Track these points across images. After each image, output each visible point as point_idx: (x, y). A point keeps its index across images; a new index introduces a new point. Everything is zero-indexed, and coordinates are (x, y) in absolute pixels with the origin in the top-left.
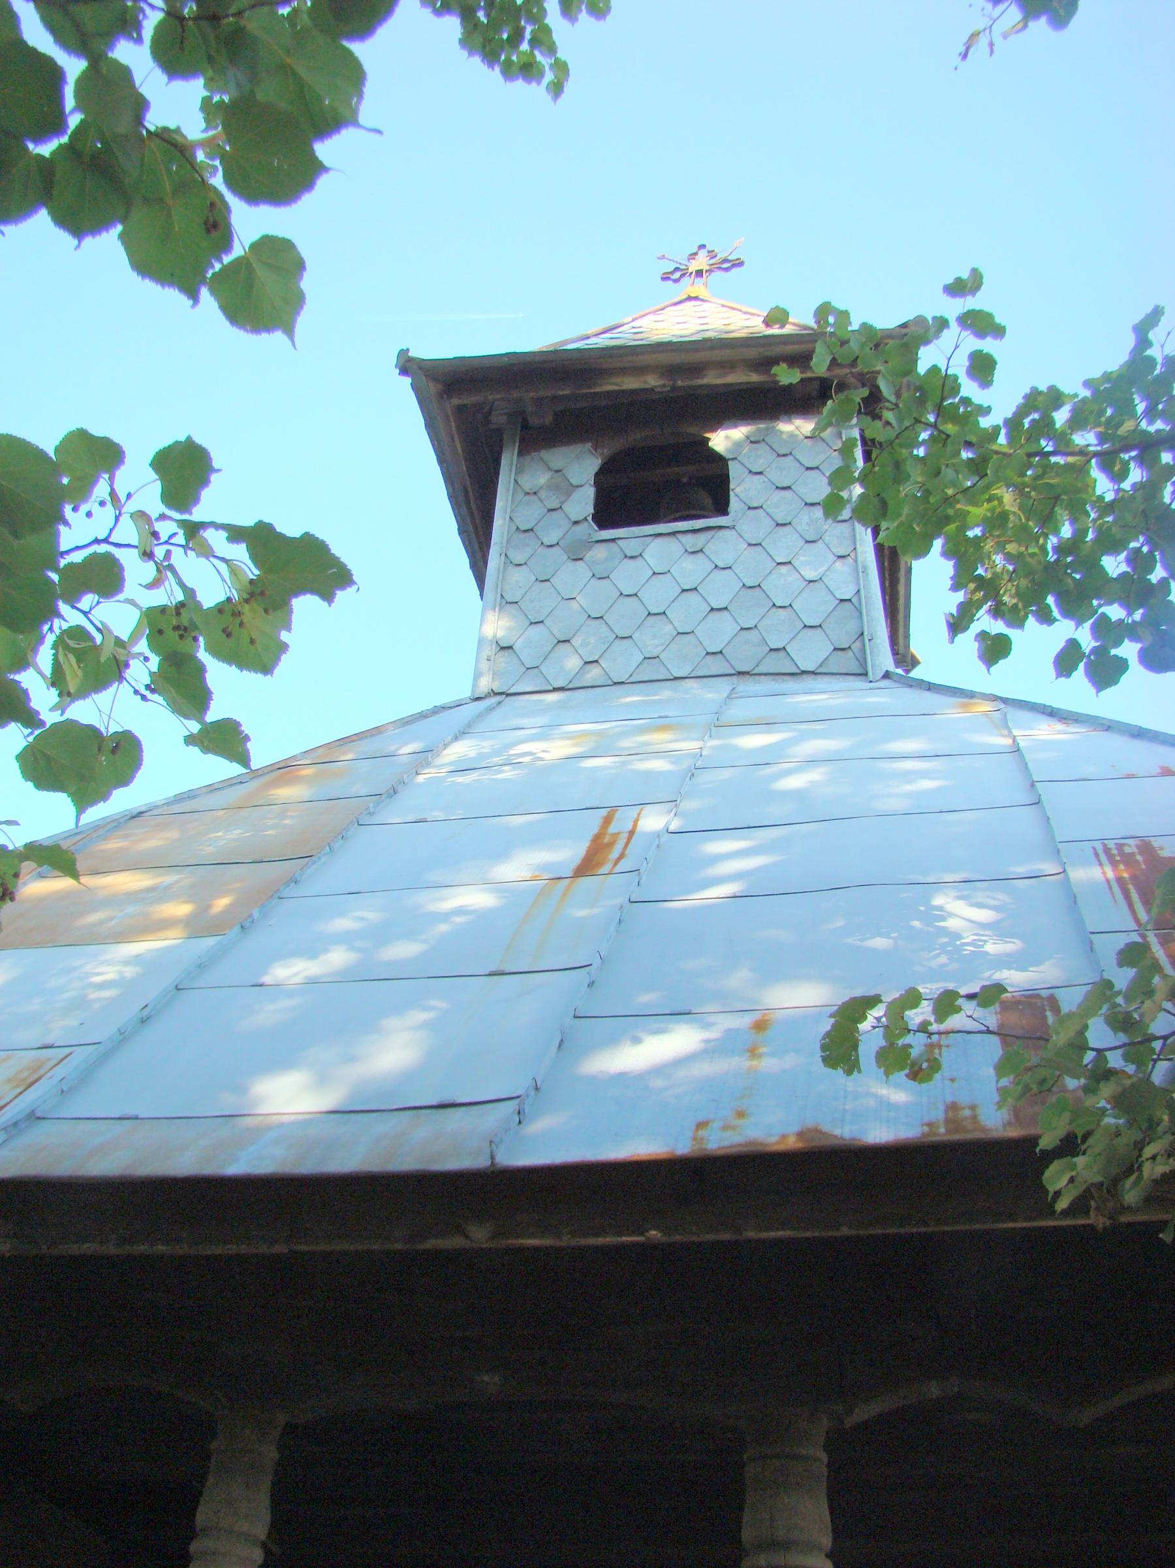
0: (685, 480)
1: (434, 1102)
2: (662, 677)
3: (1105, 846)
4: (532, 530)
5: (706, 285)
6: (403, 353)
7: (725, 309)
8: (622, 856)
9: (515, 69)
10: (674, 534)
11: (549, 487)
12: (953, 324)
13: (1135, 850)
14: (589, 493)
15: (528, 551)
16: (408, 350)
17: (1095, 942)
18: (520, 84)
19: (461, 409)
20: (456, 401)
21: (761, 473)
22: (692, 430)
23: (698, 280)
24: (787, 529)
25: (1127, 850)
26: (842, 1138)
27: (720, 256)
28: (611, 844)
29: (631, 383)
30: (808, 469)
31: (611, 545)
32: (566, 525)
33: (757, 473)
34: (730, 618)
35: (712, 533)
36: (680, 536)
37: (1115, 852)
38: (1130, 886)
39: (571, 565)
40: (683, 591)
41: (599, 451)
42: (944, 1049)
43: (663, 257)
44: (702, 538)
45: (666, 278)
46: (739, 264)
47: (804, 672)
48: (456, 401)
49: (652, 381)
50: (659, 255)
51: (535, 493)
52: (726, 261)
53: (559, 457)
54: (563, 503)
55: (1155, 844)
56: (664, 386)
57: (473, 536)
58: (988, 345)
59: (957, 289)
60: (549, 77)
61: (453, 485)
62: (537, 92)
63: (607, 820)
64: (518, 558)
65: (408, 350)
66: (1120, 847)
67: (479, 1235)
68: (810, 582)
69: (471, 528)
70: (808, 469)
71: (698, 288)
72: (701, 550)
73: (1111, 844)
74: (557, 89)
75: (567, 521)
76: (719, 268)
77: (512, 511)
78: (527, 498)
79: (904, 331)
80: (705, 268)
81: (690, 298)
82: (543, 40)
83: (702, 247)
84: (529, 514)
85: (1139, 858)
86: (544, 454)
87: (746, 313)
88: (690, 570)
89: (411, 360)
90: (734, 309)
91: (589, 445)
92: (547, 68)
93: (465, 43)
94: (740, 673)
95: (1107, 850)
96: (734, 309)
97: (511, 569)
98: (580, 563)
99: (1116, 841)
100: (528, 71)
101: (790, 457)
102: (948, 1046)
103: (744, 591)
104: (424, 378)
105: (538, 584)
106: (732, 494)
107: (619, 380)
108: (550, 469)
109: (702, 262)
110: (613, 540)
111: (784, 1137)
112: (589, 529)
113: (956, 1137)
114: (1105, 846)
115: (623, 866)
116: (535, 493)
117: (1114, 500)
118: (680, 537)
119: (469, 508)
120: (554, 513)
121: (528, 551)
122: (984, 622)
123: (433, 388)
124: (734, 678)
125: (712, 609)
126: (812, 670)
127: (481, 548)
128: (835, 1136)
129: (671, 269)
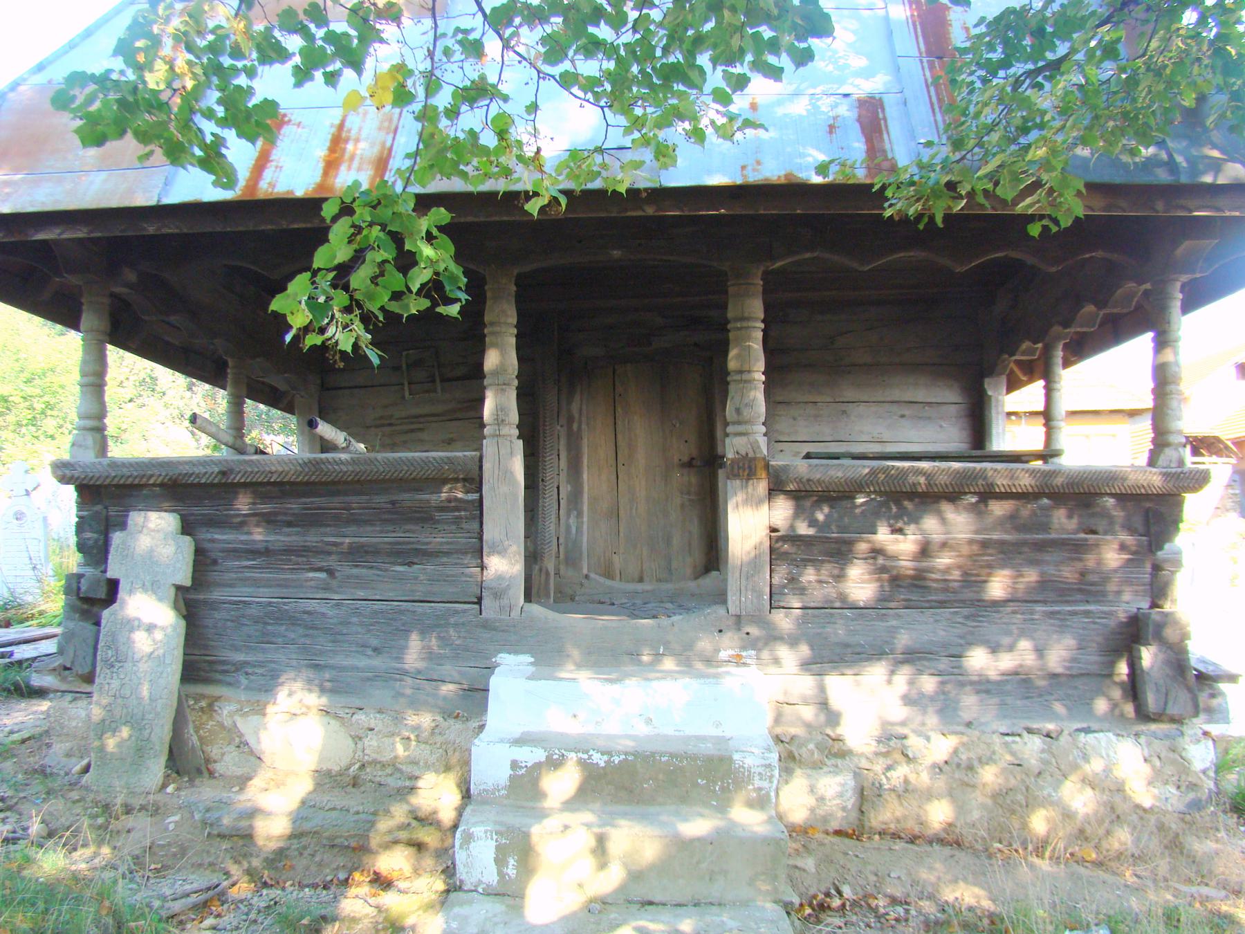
111: (779, 177)
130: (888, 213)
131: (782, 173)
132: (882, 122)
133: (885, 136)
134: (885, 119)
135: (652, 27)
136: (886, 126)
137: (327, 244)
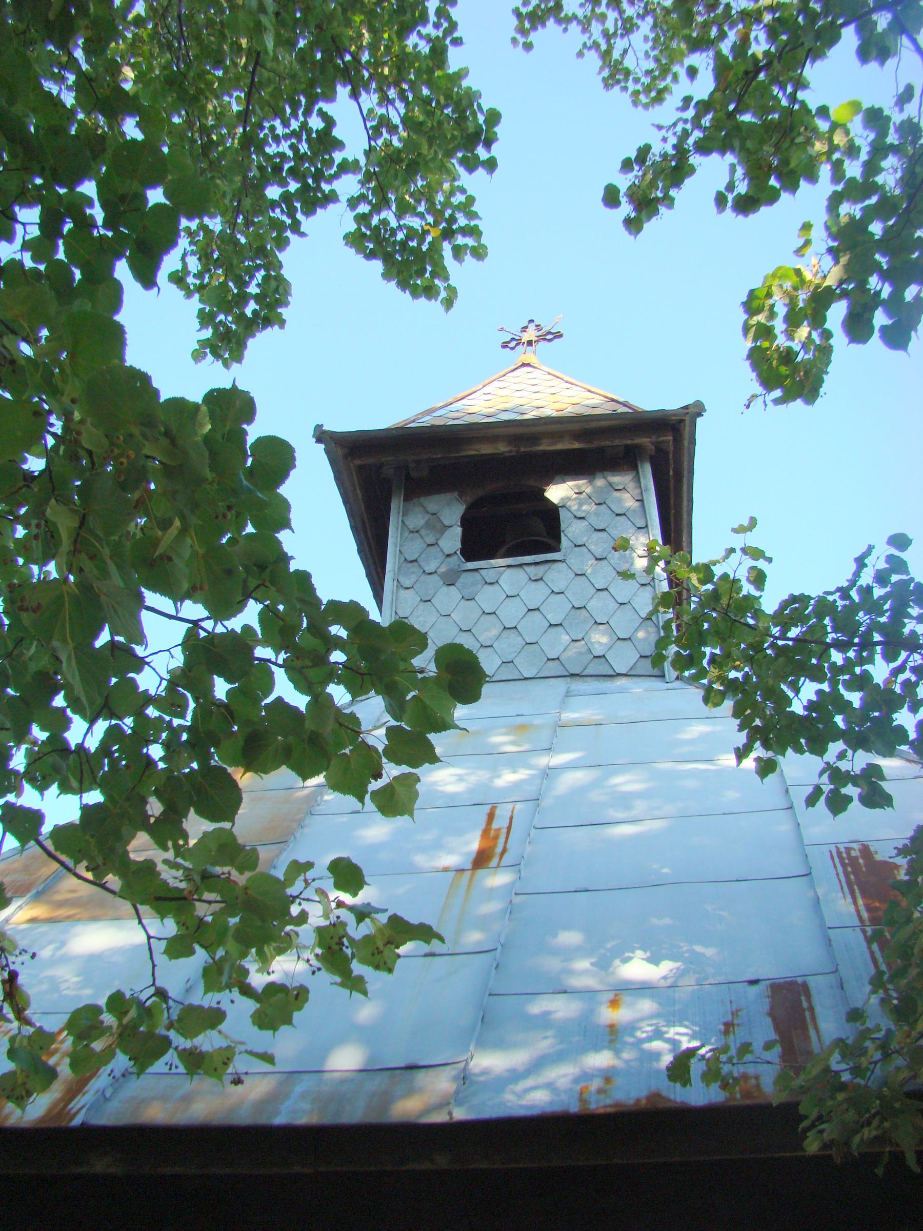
0: (525, 512)
1: (402, 1065)
2: (515, 677)
3: (837, 848)
4: (416, 561)
5: (535, 353)
6: (319, 427)
7: (551, 377)
8: (504, 850)
9: (420, 290)
10: (520, 566)
11: (427, 525)
12: (738, 552)
13: (859, 854)
14: (459, 531)
15: (413, 578)
16: (322, 425)
17: (832, 938)
18: (423, 300)
19: (360, 468)
20: (358, 462)
21: (583, 518)
22: (532, 483)
23: (529, 348)
24: (604, 563)
25: (853, 854)
26: (675, 1102)
27: (545, 329)
28: (496, 838)
29: (486, 449)
30: (618, 515)
31: (476, 574)
32: (441, 557)
33: (580, 518)
34: (564, 631)
35: (549, 565)
36: (525, 568)
37: (844, 855)
38: (856, 887)
39: (445, 589)
40: (529, 610)
41: (464, 498)
42: (736, 1028)
43: (502, 329)
44: (542, 568)
45: (505, 346)
46: (559, 335)
47: (619, 675)
48: (358, 462)
49: (502, 448)
50: (499, 328)
51: (417, 532)
52: (549, 333)
53: (433, 503)
54: (437, 540)
55: (872, 849)
56: (511, 451)
57: (369, 556)
58: (761, 564)
59: (740, 530)
60: (443, 294)
61: (354, 519)
62: (435, 306)
63: (491, 817)
64: (407, 583)
65: (322, 425)
66: (848, 850)
67: (442, 1161)
68: (621, 604)
69: (367, 549)
70: (618, 515)
71: (530, 358)
72: (542, 579)
73: (842, 849)
74: (449, 303)
75: (441, 554)
76: (545, 339)
77: (401, 545)
78: (411, 535)
79: (687, 411)
80: (534, 339)
81: (524, 365)
82: (440, 272)
83: (531, 321)
84: (414, 548)
85: (861, 861)
86: (423, 500)
87: (567, 382)
88: (534, 594)
89: (325, 432)
90: (558, 377)
91: (456, 494)
92: (442, 289)
93: (386, 276)
94: (573, 675)
95: (839, 853)
96: (558, 377)
97: (403, 593)
98: (452, 588)
99: (845, 845)
100: (429, 292)
101: (605, 506)
102: (738, 1025)
103: (573, 611)
104: (333, 445)
105: (422, 604)
106: (562, 534)
107: (477, 447)
108: (427, 512)
109: (531, 335)
110: (476, 570)
111: (638, 1100)
112: (458, 560)
113: (748, 1102)
114: (837, 848)
115: (507, 858)
116: (417, 532)
117: (843, 665)
118: (526, 568)
119: (366, 536)
120: (432, 548)
121: (413, 578)
122: (758, 751)
123: (340, 452)
124: (569, 679)
125: (551, 625)
126: (624, 672)
127: (378, 574)
128: (669, 1100)
129: (508, 339)
130: (812, 1146)
131: (644, 1093)
132: (807, 1014)
133: (812, 1032)
134: (811, 1009)
135: (152, 712)
136: (814, 1018)
137: (846, 340)
